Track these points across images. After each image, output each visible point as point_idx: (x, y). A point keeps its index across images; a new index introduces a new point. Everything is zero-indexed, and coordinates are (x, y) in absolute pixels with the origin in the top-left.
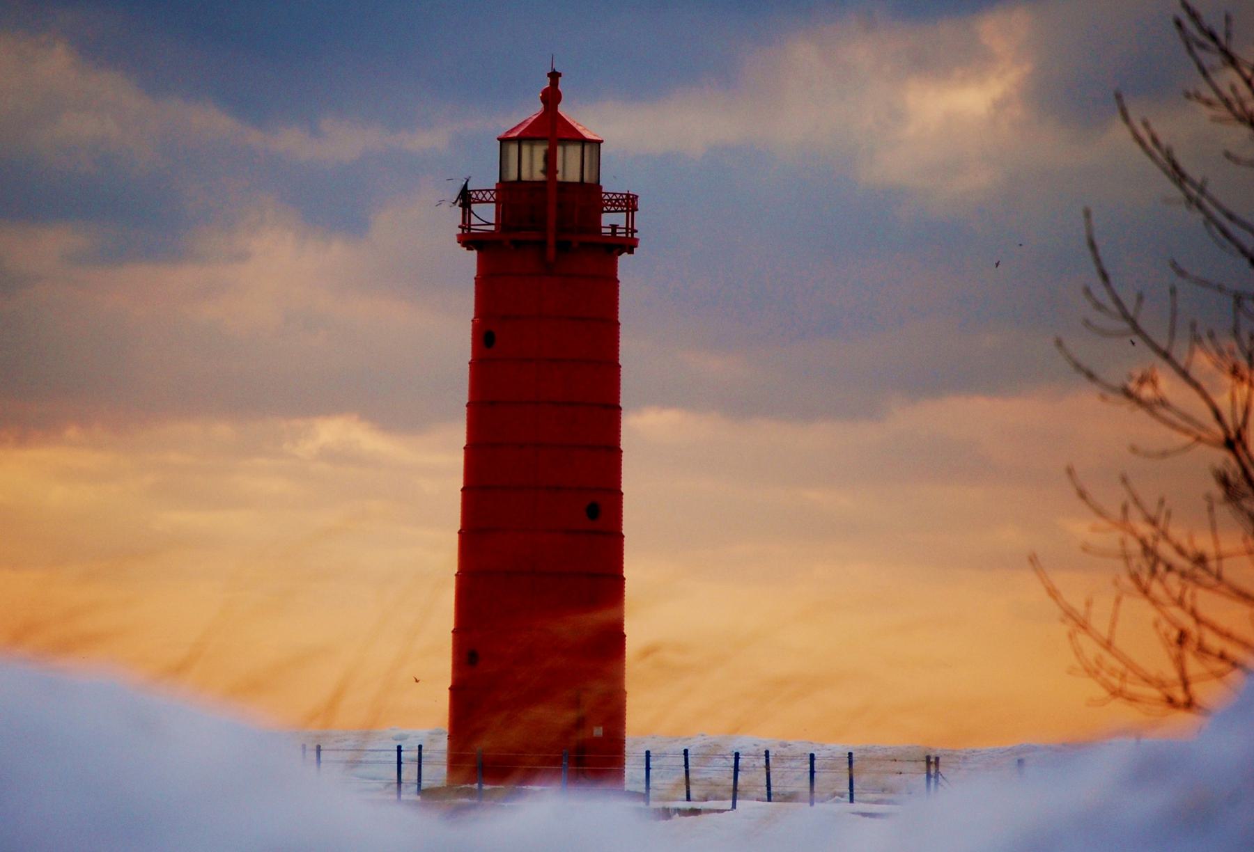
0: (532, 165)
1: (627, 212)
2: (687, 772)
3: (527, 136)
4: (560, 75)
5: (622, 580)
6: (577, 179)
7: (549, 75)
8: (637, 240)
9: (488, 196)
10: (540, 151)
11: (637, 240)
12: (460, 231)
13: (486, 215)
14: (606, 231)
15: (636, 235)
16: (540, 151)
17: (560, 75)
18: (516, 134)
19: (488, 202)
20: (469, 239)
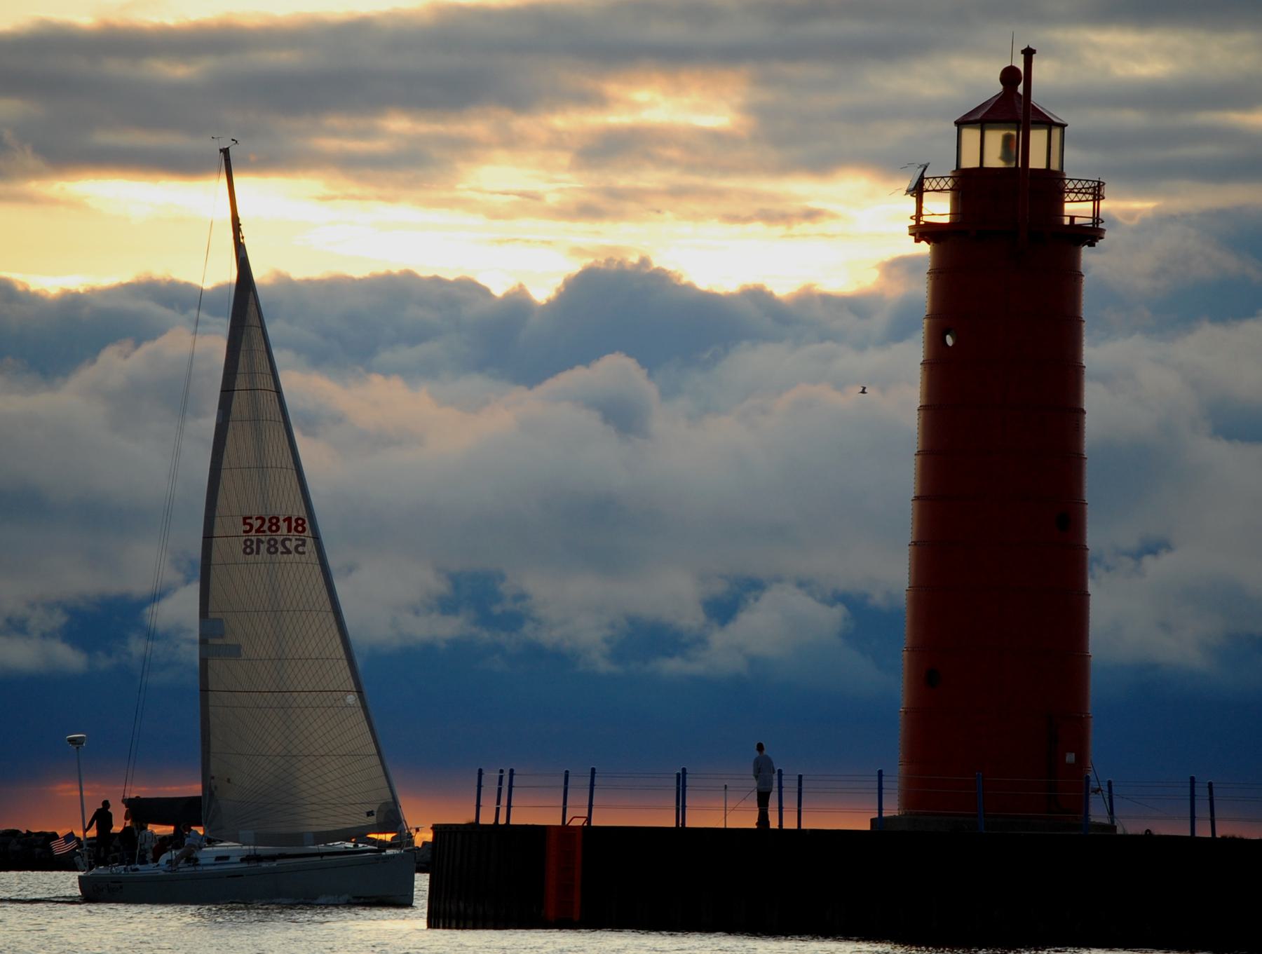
0: (991, 150)
1: (1094, 200)
2: (208, 537)
3: (982, 118)
4: (1034, 52)
5: (1085, 595)
6: (1043, 166)
7: (1023, 52)
8: (1103, 230)
9: (934, 184)
10: (995, 139)
11: (1103, 230)
12: (913, 223)
13: (939, 209)
14: (1067, 221)
15: (1101, 226)
16: (995, 139)
17: (1034, 52)
18: (979, 116)
19: (941, 190)
20: (923, 231)
